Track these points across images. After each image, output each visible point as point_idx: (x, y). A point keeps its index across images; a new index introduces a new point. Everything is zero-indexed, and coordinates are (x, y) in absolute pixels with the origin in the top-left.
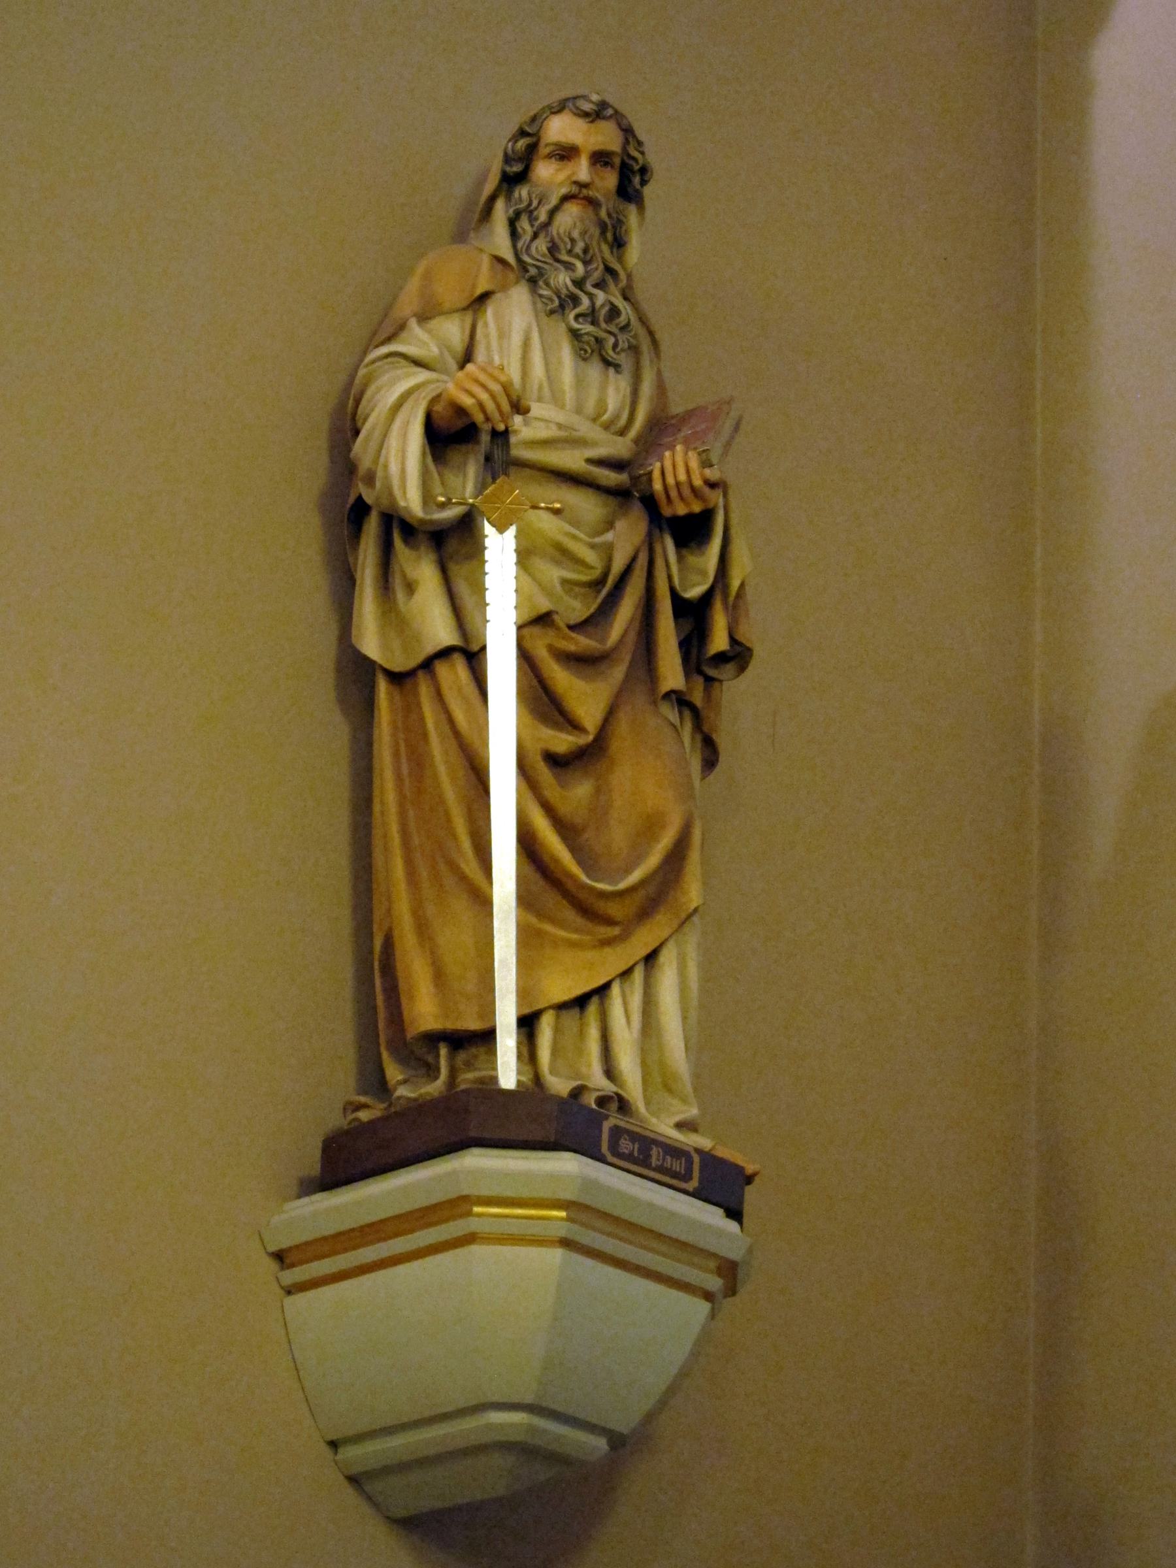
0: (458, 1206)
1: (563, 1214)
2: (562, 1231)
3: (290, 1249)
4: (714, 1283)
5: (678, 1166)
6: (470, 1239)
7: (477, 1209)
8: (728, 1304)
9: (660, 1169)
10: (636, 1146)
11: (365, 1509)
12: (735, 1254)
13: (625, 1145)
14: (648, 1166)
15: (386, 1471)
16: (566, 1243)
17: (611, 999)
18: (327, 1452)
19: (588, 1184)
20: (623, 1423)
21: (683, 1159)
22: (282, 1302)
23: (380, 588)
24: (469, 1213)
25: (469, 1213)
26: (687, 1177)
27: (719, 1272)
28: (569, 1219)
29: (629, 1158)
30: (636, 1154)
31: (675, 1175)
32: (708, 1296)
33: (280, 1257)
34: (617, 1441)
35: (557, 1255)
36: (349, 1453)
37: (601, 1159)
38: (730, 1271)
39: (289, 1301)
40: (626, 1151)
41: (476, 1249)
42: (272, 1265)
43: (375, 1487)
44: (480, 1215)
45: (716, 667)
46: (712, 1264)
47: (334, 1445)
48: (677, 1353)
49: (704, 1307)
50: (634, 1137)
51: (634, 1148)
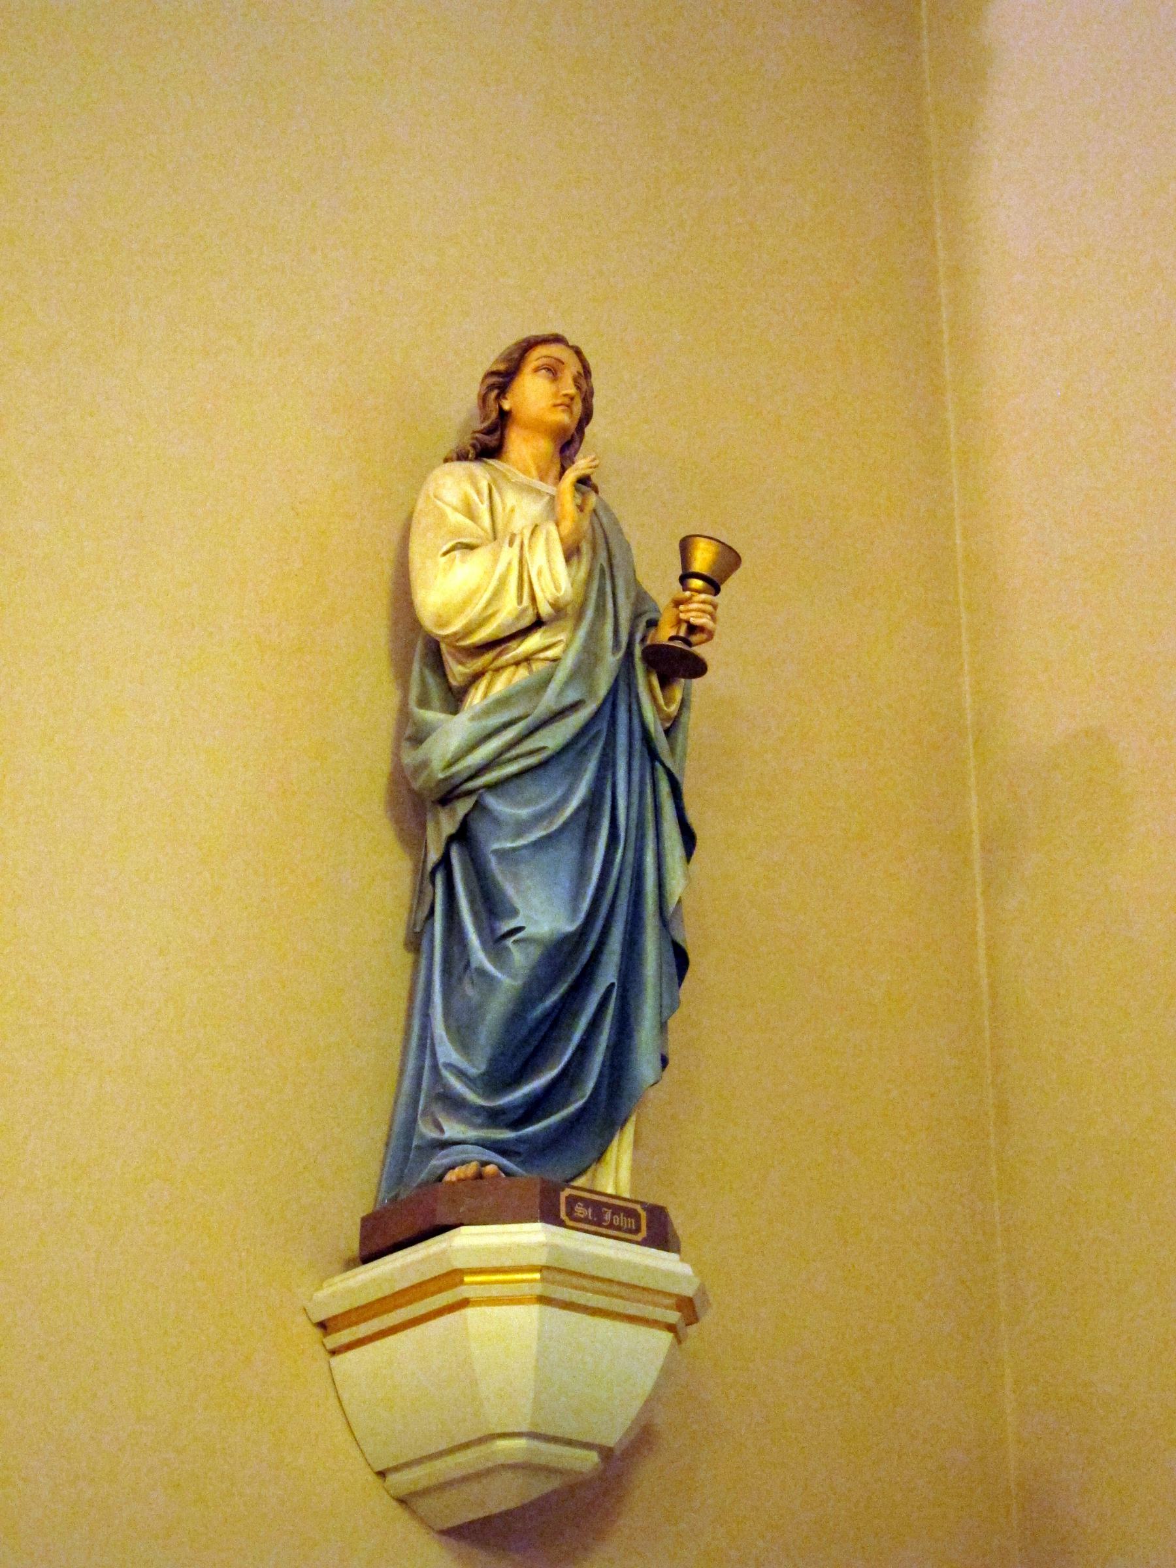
0: (453, 1277)
1: (537, 1276)
2: (538, 1289)
3: (329, 1319)
4: (673, 1317)
5: (631, 1223)
6: (464, 1303)
7: (467, 1279)
8: (693, 1330)
9: (611, 1226)
10: (590, 1210)
11: (414, 1525)
12: (689, 1291)
13: (580, 1210)
14: (599, 1224)
15: (426, 1492)
16: (543, 1300)
17: (433, 1003)
18: (378, 1481)
19: (553, 1248)
20: (612, 1437)
21: (622, 1214)
22: (329, 1362)
23: (628, 1070)
24: (462, 1282)
25: (462, 1282)
26: (638, 1230)
27: (679, 1308)
28: (542, 1280)
29: (585, 1220)
30: (590, 1218)
31: (630, 1231)
32: (671, 1328)
33: (323, 1325)
34: (606, 1453)
35: (535, 1309)
36: (392, 1478)
37: (561, 1224)
38: (689, 1308)
39: (336, 1361)
40: (582, 1216)
41: (469, 1311)
42: (317, 1333)
43: (424, 1505)
44: (472, 1283)
45: (561, 589)
46: (670, 1301)
47: (382, 1474)
48: (646, 1382)
49: (667, 1337)
50: (588, 1203)
51: (588, 1213)
